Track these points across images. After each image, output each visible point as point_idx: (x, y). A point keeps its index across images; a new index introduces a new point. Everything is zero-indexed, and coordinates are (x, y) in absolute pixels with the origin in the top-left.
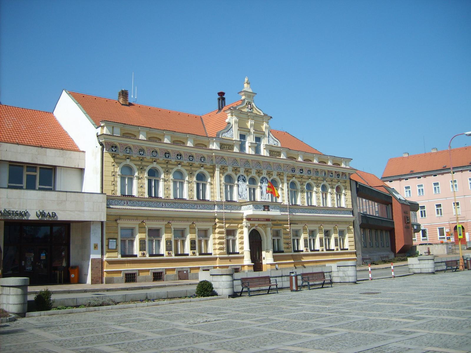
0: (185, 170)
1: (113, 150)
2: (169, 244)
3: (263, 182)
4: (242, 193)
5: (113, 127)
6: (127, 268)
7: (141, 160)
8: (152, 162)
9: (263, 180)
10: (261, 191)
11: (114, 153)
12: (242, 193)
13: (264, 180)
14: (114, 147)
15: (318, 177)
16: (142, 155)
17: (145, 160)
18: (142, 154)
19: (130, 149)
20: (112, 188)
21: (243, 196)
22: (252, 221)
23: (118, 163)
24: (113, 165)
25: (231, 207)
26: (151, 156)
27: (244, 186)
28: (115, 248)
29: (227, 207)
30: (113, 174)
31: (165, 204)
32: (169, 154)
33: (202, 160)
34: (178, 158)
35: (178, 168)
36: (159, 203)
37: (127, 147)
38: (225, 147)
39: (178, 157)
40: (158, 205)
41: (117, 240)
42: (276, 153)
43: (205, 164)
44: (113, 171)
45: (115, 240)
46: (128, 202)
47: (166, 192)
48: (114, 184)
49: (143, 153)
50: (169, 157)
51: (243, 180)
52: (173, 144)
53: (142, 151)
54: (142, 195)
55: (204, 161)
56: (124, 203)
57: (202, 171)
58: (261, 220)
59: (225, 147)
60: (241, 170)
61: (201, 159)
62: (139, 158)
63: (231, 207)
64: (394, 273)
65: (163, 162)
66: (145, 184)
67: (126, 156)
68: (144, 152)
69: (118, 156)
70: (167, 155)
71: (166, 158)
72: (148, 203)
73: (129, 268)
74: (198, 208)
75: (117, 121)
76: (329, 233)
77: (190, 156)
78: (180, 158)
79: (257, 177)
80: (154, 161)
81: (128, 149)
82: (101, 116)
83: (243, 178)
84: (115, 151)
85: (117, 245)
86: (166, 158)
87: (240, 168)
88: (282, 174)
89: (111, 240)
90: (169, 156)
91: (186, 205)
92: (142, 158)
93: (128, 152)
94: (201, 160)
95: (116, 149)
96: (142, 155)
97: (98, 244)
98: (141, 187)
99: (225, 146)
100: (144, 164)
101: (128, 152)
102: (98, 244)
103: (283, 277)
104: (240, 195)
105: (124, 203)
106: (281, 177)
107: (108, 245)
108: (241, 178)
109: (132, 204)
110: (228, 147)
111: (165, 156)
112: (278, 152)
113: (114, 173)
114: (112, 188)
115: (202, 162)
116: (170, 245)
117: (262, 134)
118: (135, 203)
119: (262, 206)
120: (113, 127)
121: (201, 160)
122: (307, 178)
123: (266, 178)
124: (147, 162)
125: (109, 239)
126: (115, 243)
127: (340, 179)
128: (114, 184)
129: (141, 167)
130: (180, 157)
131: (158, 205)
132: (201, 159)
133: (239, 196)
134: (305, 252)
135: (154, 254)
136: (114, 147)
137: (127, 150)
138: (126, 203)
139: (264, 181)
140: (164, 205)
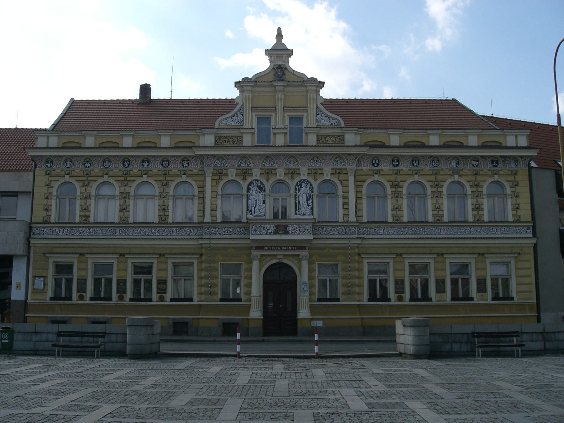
0: (154, 182)
1: (47, 166)
2: (121, 284)
3: (301, 187)
4: (255, 208)
5: (516, 136)
6: (466, 314)
7: (87, 174)
8: (412, 175)
9: (301, 185)
10: (296, 203)
11: (49, 169)
12: (255, 208)
13: (303, 184)
14: (49, 162)
15: (438, 170)
16: (89, 167)
17: (92, 173)
18: (87, 167)
19: (70, 161)
20: (44, 213)
21: (257, 212)
22: (266, 250)
23: (158, 181)
24: (47, 184)
25: (72, 230)
26: (152, 167)
27: (261, 196)
28: (42, 288)
29: (224, 230)
30: (46, 196)
31: (119, 230)
32: (129, 161)
33: (185, 164)
34: (143, 165)
35: (301, 177)
36: (110, 229)
37: (68, 160)
38: (227, 140)
39: (143, 164)
40: (109, 232)
41: (46, 278)
42: (333, 139)
43: (170, 169)
44: (47, 192)
45: (42, 279)
46: (121, 231)
47: (122, 214)
48: (46, 209)
49: (89, 165)
50: (130, 166)
51: (259, 187)
52: (216, 147)
53: (87, 163)
54: (85, 220)
55: (188, 165)
56: (59, 232)
57: (282, 179)
58: (285, 248)
59: (227, 140)
60: (253, 173)
61: (183, 163)
62: (84, 171)
63: (72, 230)
64: (241, 348)
65: (120, 173)
66: (90, 205)
67: (373, 171)
68: (90, 164)
69: (53, 173)
70: (126, 164)
71: (125, 167)
72: (362, 229)
73: (468, 314)
74: (174, 234)
75: (404, 126)
76: (470, 269)
77: (163, 161)
78: (148, 165)
79: (289, 182)
80: (375, 174)
81: (68, 163)
82: (450, 125)
83: (259, 184)
84: (51, 166)
85: (45, 284)
86: (125, 167)
87: (251, 169)
88: (344, 172)
89: (37, 278)
90: (129, 165)
91: (364, 229)
92: (396, 171)
93: (68, 166)
94: (183, 165)
95: (52, 164)
96: (89, 167)
97: (21, 283)
98: (85, 209)
99: (230, 140)
100: (399, 178)
101: (68, 166)
102: (21, 283)
103: (81, 341)
104: (251, 211)
105: (116, 233)
106: (342, 177)
107: (33, 284)
108: (255, 184)
109: (126, 232)
110: (231, 140)
111: (124, 165)
112: (339, 136)
113: (47, 194)
114: (44, 213)
115: (185, 167)
116: (123, 286)
117: (271, 111)
118: (131, 231)
119: (272, 226)
120: (516, 136)
121: (183, 165)
122: (410, 172)
123: (307, 181)
124: (173, 176)
125: (34, 277)
126: (43, 282)
127: (500, 169)
128: (47, 208)
129: (436, 183)
130: (148, 164)
131: (109, 232)
132: (183, 163)
133: (249, 213)
134: (131, 300)
135: (328, 297)
136: (49, 162)
137: (67, 163)
138: (62, 231)
139: (303, 186)
140: (118, 232)
